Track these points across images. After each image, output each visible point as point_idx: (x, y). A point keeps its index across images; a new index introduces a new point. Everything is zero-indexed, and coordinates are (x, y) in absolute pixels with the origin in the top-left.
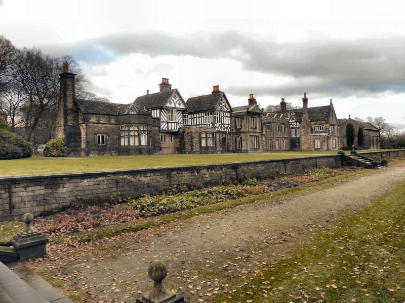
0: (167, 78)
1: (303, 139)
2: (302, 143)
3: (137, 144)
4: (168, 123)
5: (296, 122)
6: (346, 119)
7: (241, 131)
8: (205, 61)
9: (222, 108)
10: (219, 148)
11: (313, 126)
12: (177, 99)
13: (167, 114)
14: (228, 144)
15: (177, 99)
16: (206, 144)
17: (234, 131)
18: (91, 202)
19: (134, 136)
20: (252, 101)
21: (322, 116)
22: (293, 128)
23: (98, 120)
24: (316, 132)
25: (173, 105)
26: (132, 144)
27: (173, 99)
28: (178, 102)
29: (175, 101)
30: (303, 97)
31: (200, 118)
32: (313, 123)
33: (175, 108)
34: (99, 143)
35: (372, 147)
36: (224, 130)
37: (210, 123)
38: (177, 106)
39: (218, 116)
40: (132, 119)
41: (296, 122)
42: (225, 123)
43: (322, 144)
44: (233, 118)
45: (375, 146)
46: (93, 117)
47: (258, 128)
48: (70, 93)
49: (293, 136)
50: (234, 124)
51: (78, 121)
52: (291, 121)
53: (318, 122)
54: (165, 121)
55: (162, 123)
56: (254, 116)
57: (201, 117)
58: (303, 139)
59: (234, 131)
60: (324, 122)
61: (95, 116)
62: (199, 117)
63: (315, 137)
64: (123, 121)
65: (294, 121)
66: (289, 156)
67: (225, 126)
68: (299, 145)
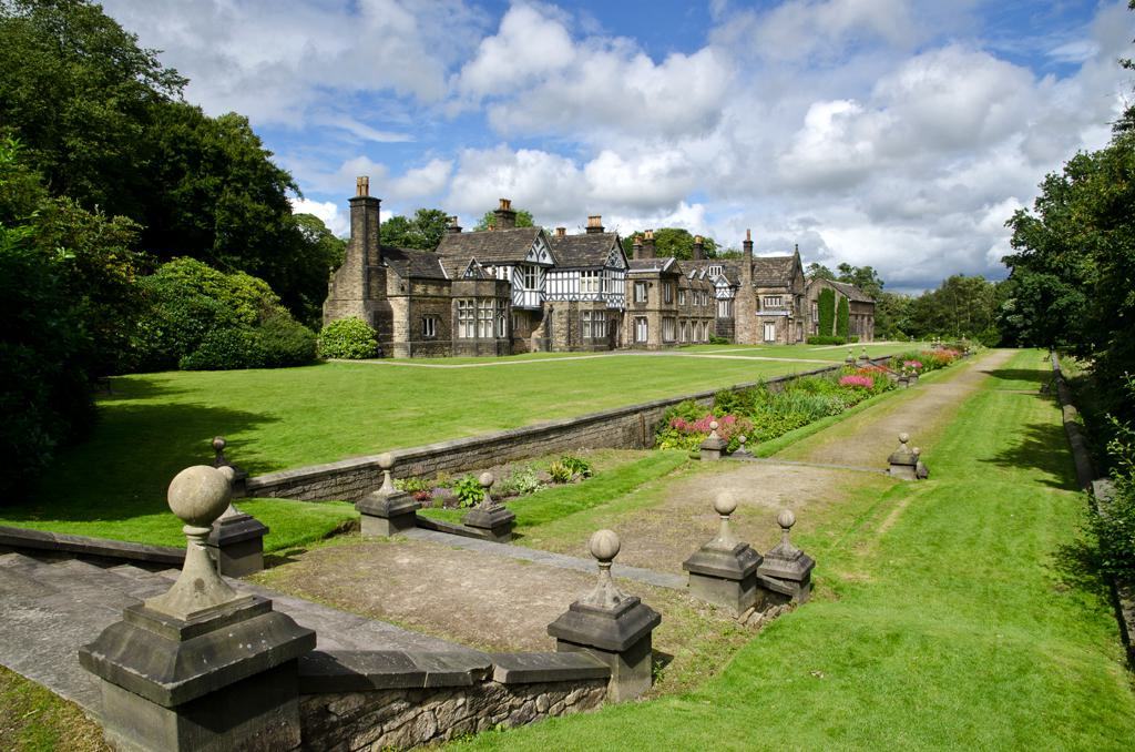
1: (741, 321)
4: (524, 292)
7: (647, 307)
8: (315, 215)
11: (761, 297)
12: (541, 246)
15: (541, 246)
16: (593, 334)
17: (632, 307)
20: (748, 244)
22: (722, 300)
23: (425, 290)
24: (766, 309)
25: (534, 259)
26: (482, 335)
29: (538, 249)
30: (745, 238)
31: (571, 282)
32: (760, 290)
33: (538, 263)
34: (426, 333)
40: (482, 287)
41: (730, 287)
44: (631, 282)
45: (865, 336)
47: (767, 313)
49: (722, 312)
50: (631, 294)
52: (719, 285)
53: (772, 290)
58: (741, 321)
59: (632, 307)
60: (784, 289)
61: (420, 281)
62: (568, 279)
63: (766, 319)
65: (725, 285)
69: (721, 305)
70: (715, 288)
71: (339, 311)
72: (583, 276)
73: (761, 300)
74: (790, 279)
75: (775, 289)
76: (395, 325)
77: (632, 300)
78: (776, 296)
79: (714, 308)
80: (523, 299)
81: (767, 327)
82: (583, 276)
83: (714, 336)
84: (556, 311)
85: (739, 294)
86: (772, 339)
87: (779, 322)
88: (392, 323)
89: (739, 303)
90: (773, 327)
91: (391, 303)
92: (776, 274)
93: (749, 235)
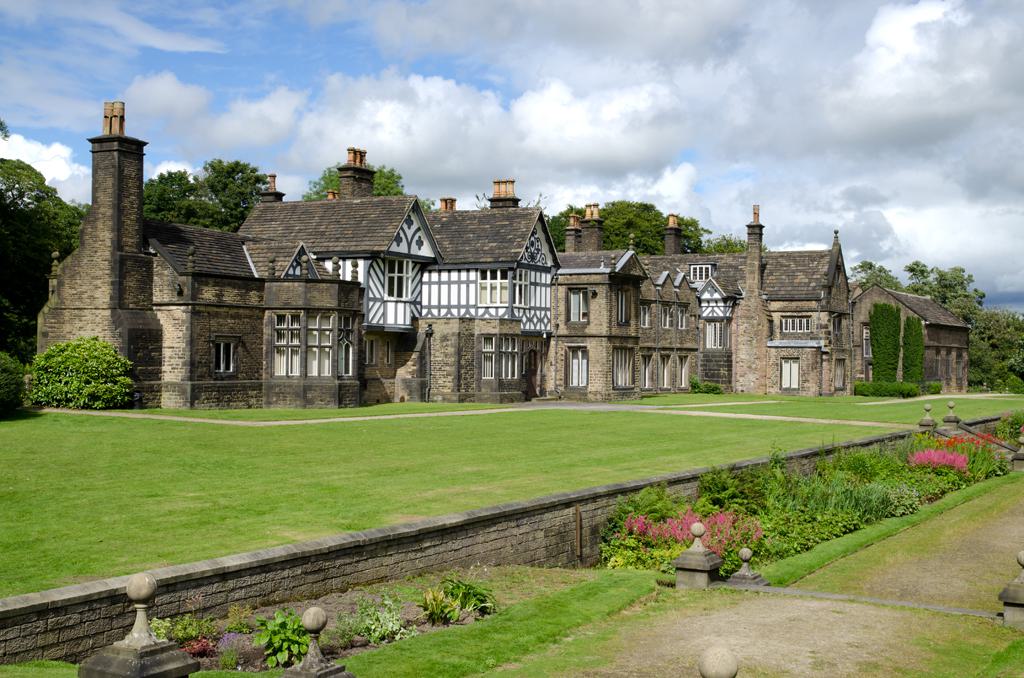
0: (362, 149)
2: (737, 369)
3: (296, 372)
5: (725, 300)
6: (661, 214)
9: (532, 257)
10: (392, 381)
11: (776, 317)
12: (414, 227)
13: (384, 275)
14: (347, 347)
15: (414, 227)
17: (563, 330)
18: (877, 442)
19: (321, 348)
21: (808, 285)
22: (710, 320)
23: (219, 296)
24: (784, 336)
25: (403, 248)
27: (405, 227)
28: (416, 238)
29: (410, 233)
32: (775, 305)
33: (409, 256)
35: (945, 389)
36: (535, 326)
37: (498, 304)
38: (415, 251)
39: (523, 283)
40: (315, 294)
41: (725, 300)
42: (408, 305)
43: (803, 380)
44: (562, 290)
45: (953, 383)
46: (207, 285)
48: (132, 203)
49: (711, 342)
51: (151, 294)
52: (706, 296)
53: (794, 304)
54: (378, 296)
55: (371, 304)
56: (626, 287)
57: (468, 282)
59: (563, 330)
60: (814, 304)
61: (211, 281)
63: (784, 353)
64: (284, 297)
65: (717, 296)
66: (198, 417)
67: (538, 313)
68: (730, 376)
69: (710, 329)
70: (700, 301)
71: (67, 328)
72: (484, 277)
73: (777, 322)
74: (824, 287)
75: (799, 303)
76: (167, 353)
77: (562, 318)
78: (801, 315)
79: (698, 334)
80: (384, 315)
81: (786, 366)
82: (484, 277)
83: (697, 379)
84: (437, 335)
85: (739, 311)
86: (795, 385)
87: (807, 357)
88: (159, 349)
89: (739, 327)
90: (795, 366)
91: (160, 315)
92: (801, 278)
93: (756, 214)
